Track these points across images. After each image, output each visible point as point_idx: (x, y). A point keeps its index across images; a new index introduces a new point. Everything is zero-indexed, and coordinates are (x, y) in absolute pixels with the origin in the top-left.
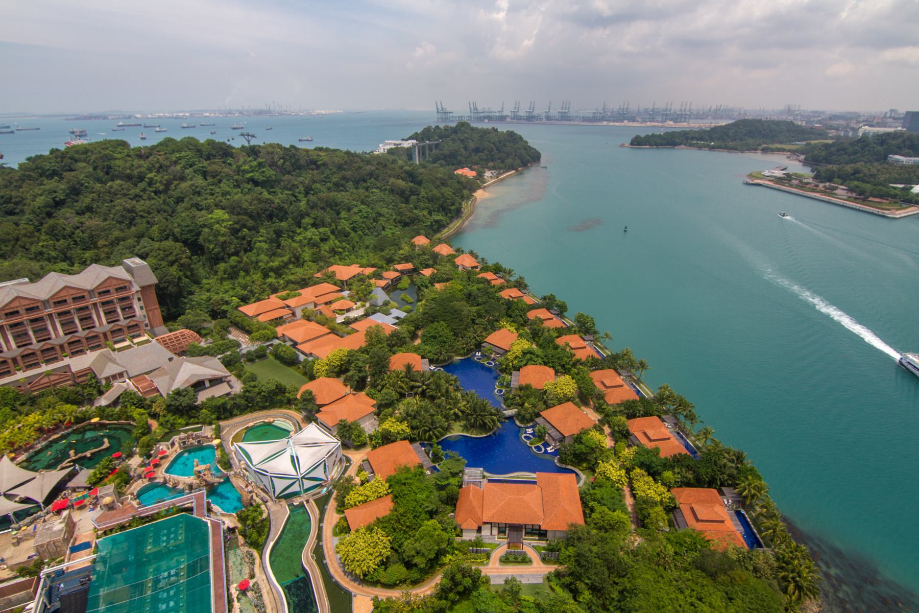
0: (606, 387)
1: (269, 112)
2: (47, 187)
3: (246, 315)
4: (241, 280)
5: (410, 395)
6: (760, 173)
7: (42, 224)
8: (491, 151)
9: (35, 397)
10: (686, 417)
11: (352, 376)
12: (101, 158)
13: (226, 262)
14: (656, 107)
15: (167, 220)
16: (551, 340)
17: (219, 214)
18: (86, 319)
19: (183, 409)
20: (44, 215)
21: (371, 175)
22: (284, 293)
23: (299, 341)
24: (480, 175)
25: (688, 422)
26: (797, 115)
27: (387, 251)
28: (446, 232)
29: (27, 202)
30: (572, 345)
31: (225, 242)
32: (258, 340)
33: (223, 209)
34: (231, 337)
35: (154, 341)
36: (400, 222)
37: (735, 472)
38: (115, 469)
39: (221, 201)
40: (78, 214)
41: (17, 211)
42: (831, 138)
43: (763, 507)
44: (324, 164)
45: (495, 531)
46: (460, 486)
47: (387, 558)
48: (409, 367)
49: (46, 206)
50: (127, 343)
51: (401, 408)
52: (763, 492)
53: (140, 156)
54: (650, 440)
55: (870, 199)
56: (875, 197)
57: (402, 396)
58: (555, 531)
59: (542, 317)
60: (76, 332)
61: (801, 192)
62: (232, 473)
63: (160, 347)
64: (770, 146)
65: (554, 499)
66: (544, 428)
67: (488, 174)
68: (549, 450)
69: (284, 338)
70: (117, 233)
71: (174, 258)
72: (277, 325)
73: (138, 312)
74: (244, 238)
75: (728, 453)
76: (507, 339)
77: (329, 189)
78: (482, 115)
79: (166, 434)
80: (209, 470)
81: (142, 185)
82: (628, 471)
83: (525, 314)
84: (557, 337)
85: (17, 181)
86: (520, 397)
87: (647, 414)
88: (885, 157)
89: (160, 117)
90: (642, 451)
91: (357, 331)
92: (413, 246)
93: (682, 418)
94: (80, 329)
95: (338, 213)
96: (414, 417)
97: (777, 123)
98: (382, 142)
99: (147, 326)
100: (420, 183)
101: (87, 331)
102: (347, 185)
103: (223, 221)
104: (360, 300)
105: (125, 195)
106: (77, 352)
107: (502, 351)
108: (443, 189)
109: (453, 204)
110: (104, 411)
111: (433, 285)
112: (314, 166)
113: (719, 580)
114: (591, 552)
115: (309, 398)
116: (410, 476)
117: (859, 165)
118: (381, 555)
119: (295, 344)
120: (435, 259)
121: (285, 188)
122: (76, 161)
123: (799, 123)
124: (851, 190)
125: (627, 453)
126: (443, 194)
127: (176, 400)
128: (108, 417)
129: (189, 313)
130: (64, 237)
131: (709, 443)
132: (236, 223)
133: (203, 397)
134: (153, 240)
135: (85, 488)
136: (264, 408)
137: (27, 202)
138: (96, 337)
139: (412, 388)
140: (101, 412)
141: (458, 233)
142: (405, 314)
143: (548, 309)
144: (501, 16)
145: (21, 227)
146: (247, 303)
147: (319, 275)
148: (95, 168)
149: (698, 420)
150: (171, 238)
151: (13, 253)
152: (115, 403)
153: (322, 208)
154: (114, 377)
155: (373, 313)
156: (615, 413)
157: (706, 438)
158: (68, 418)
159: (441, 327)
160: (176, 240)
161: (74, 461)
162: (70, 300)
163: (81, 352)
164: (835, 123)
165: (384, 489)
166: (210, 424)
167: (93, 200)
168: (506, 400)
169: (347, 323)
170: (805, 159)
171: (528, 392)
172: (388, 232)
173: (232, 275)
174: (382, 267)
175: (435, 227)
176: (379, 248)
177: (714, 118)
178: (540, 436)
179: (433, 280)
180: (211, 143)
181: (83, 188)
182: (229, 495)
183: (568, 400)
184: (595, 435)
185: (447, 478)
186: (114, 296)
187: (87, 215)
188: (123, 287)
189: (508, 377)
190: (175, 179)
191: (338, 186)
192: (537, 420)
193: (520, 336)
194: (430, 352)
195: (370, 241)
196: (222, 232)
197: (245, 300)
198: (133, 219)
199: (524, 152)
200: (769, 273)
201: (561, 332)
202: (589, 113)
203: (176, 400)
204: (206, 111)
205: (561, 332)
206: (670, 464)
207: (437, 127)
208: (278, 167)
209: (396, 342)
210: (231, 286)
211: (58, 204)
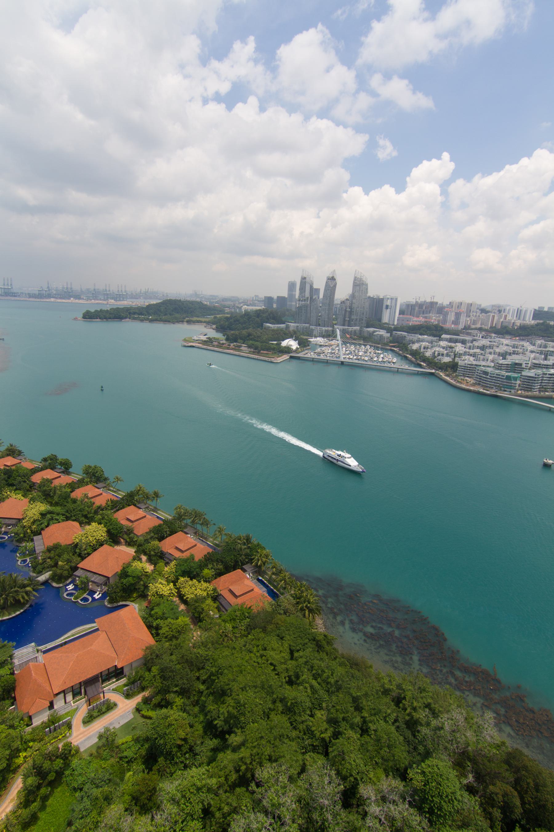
6: (191, 338)
16: (66, 497)
25: (205, 528)
26: (202, 297)
37: (248, 551)
42: (228, 313)
43: (273, 567)
45: (69, 697)
46: (13, 674)
55: (262, 352)
58: (131, 664)
59: (49, 477)
65: (125, 635)
66: (87, 578)
75: (240, 539)
82: (175, 582)
83: (28, 479)
84: (71, 492)
87: (173, 532)
88: (262, 325)
90: (181, 562)
93: (199, 527)
97: (192, 303)
107: (14, 522)
113: (269, 629)
114: (173, 662)
117: (250, 330)
123: (206, 303)
124: (249, 347)
131: (224, 537)
143: (52, 469)
149: (212, 523)
156: (147, 541)
157: (221, 534)
164: (227, 303)
170: (216, 327)
171: (58, 551)
177: (145, 298)
178: (83, 587)
184: (137, 565)
189: (29, 545)
205: (73, 486)
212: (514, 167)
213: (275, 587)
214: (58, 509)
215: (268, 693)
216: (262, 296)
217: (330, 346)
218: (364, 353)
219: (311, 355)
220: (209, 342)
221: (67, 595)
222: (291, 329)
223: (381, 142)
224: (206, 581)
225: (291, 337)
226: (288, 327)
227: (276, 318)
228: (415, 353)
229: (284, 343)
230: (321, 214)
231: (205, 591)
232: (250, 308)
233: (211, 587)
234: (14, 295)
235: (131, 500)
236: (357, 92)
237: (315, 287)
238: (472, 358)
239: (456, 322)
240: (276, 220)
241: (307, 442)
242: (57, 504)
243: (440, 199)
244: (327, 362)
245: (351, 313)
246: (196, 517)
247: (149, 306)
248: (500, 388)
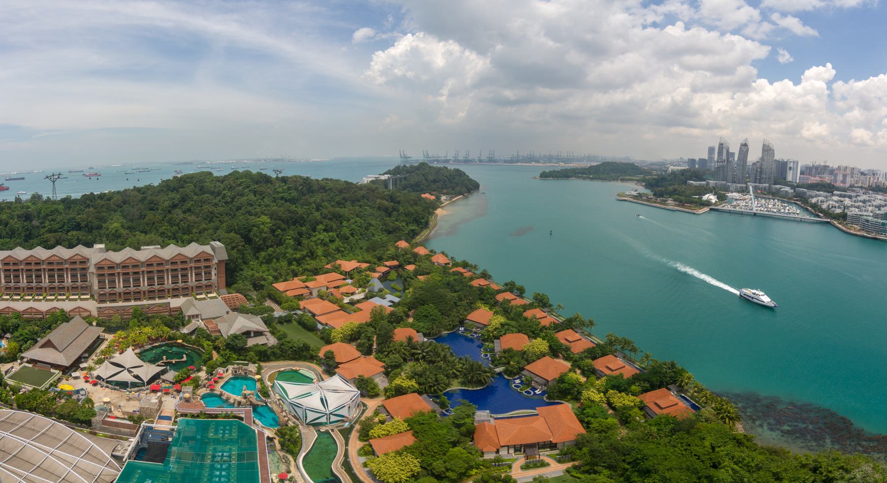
1: (282, 160)
5: (411, 360)
11: (364, 343)
16: (520, 315)
17: (265, 218)
19: (236, 348)
21: (363, 197)
22: (304, 277)
24: (438, 198)
25: (633, 354)
28: (418, 239)
47: (418, 473)
48: (410, 339)
50: (203, 296)
54: (612, 370)
63: (223, 302)
67: (443, 198)
68: (537, 392)
70: (204, 226)
73: (214, 277)
76: (483, 316)
81: (219, 198)
82: (605, 393)
90: (610, 379)
92: (397, 248)
93: (627, 352)
97: (626, 164)
104: (360, 286)
108: (416, 208)
115: (330, 356)
117: (676, 186)
118: (412, 470)
119: (314, 315)
120: (415, 258)
124: (675, 200)
132: (274, 225)
133: (251, 342)
153: (330, 219)
154: (193, 316)
155: (371, 297)
156: (581, 359)
159: (431, 309)
160: (236, 233)
163: (176, 296)
165: (404, 426)
169: (352, 303)
173: (268, 261)
174: (375, 263)
176: (371, 249)
179: (417, 273)
183: (544, 355)
197: (276, 279)
202: (508, 157)
205: (526, 308)
209: (396, 320)
211: (175, 206)
212: (876, 79)
213: (697, 402)
214: (513, 323)
215: (693, 473)
216: (686, 158)
217: (744, 199)
218: (773, 206)
219: (728, 207)
220: (639, 196)
222: (711, 185)
223: (781, 52)
224: (633, 395)
225: (711, 192)
226: (708, 184)
227: (698, 176)
228: (814, 206)
229: (705, 197)
230: (735, 96)
232: (676, 168)
233: (638, 399)
234: (495, 161)
235: (569, 324)
236: (762, 21)
237: (731, 151)
238: (857, 210)
239: (844, 182)
240: (698, 100)
241: (725, 283)
242: (512, 319)
243: (826, 92)
244: (742, 214)
245: (761, 172)
248: (878, 232)
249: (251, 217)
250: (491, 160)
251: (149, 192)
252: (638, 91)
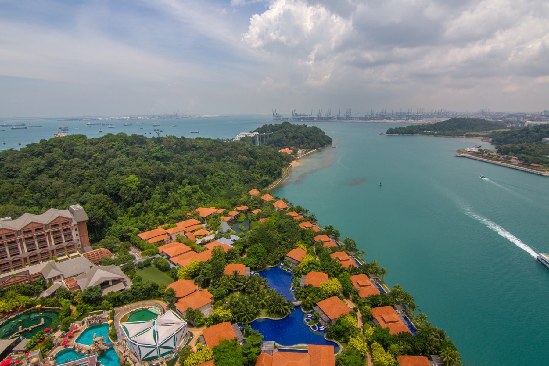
0: (360, 286)
1: (176, 116)
2: (34, 162)
3: (142, 239)
4: (142, 217)
7: (27, 184)
8: (302, 138)
9: (5, 291)
10: (409, 306)
12: (69, 145)
13: (134, 206)
14: (402, 111)
15: (102, 181)
17: (133, 177)
18: (42, 242)
19: (93, 300)
20: (30, 178)
21: (227, 153)
23: (171, 256)
24: (295, 153)
26: (488, 115)
27: (233, 199)
28: (271, 187)
29: (21, 170)
30: (341, 258)
31: (134, 194)
32: (146, 255)
33: (136, 174)
34: (131, 253)
35: (82, 255)
36: (243, 181)
38: (44, 339)
39: (135, 170)
40: (50, 177)
41: (14, 176)
42: (508, 128)
44: (200, 147)
48: (236, 273)
49: (32, 173)
50: (66, 257)
51: (227, 301)
52: (456, 359)
53: (92, 144)
55: (532, 164)
56: (535, 163)
57: (231, 291)
59: (323, 240)
60: (35, 250)
61: (489, 161)
62: (117, 343)
64: (471, 133)
66: (318, 314)
67: (300, 151)
69: (163, 254)
70: (70, 189)
71: (102, 204)
72: (160, 245)
73: (75, 237)
74: (146, 192)
75: (435, 332)
76: (300, 254)
77: (202, 162)
78: (300, 117)
79: (81, 316)
80: (103, 340)
81: (90, 161)
82: (369, 344)
83: (313, 238)
84: (332, 253)
85: (18, 158)
86: (305, 293)
87: (384, 305)
88: (541, 139)
89: (112, 119)
90: (379, 330)
91: (208, 249)
92: (249, 196)
94: (38, 248)
95: (205, 176)
96: (236, 306)
98: (239, 133)
99: (79, 246)
100: (256, 158)
101: (42, 249)
102: (213, 159)
103: (134, 181)
104: (212, 229)
105: (79, 167)
106: (35, 262)
107: (296, 262)
109: (276, 170)
110: (44, 300)
111: (258, 220)
112: (194, 149)
116: (227, 346)
117: (523, 144)
119: (169, 257)
120: (261, 203)
121: (176, 162)
122: (54, 147)
123: (489, 120)
124: (520, 159)
125: (370, 330)
126: (270, 165)
127: (89, 294)
128: (46, 305)
129: (107, 238)
130: (40, 192)
131: (423, 324)
132: (142, 183)
134: (91, 193)
135: (24, 351)
136: (144, 299)
137: (21, 170)
138: (47, 253)
139: (237, 286)
140: (43, 299)
141: (280, 187)
142: (238, 238)
143: (328, 235)
144: (311, 62)
145: (15, 185)
146: (144, 231)
147: (189, 214)
148: (64, 151)
149: (417, 308)
150: (102, 192)
151: (7, 201)
152: (52, 295)
153: (196, 173)
154: (55, 278)
155: (220, 238)
158: (22, 304)
159: (259, 247)
160: (105, 193)
161: (20, 333)
162: (33, 230)
163: (36, 262)
164: (511, 119)
166: (108, 309)
167: (60, 169)
168: (296, 294)
169: (203, 244)
172: (235, 187)
173: (137, 214)
174: (229, 209)
175: (264, 184)
176: (228, 197)
177: (438, 117)
178: (316, 319)
179: (259, 217)
180: (134, 136)
181: (55, 162)
182: (113, 358)
183: (335, 295)
184: (350, 319)
185: (249, 348)
186: (61, 228)
187: (56, 178)
188: (67, 222)
190: (110, 157)
191: (207, 160)
192: (315, 308)
193: (308, 252)
194: (251, 263)
195: (224, 192)
196: (133, 188)
197: (142, 229)
198: (82, 180)
199: (321, 138)
200: (468, 211)
201: (334, 250)
202: (363, 115)
203: (89, 294)
204: (139, 116)
205: (334, 250)
206: (395, 340)
207: (271, 125)
208: (173, 149)
209: (230, 256)
210: (135, 221)
211: (39, 172)
220: (481, 153)
221: (307, 320)
231: (388, 361)
246: (405, 299)
247: (437, 124)
249: (121, 177)
250: (348, 118)
251: (8, 158)
252: (500, 40)
